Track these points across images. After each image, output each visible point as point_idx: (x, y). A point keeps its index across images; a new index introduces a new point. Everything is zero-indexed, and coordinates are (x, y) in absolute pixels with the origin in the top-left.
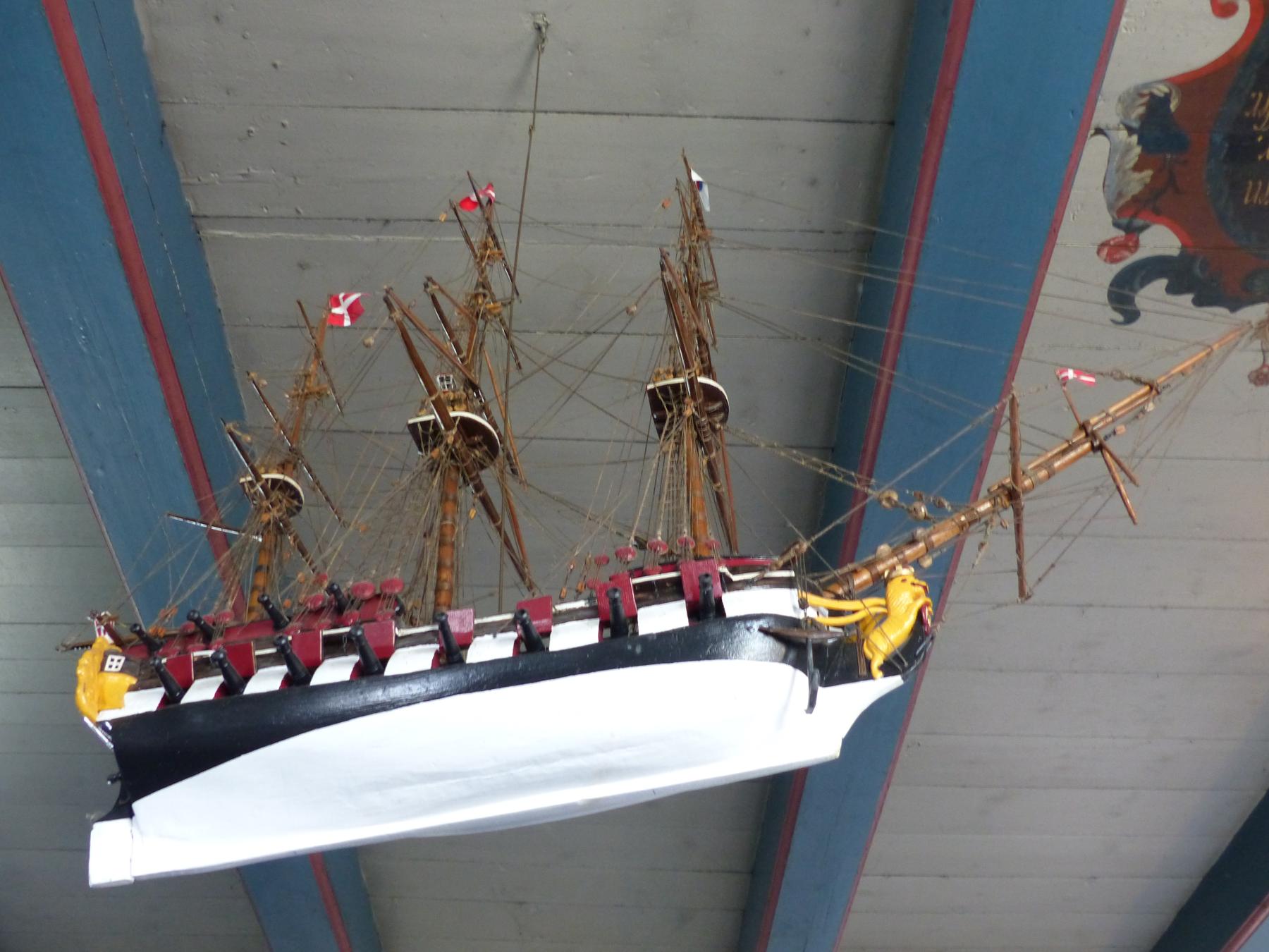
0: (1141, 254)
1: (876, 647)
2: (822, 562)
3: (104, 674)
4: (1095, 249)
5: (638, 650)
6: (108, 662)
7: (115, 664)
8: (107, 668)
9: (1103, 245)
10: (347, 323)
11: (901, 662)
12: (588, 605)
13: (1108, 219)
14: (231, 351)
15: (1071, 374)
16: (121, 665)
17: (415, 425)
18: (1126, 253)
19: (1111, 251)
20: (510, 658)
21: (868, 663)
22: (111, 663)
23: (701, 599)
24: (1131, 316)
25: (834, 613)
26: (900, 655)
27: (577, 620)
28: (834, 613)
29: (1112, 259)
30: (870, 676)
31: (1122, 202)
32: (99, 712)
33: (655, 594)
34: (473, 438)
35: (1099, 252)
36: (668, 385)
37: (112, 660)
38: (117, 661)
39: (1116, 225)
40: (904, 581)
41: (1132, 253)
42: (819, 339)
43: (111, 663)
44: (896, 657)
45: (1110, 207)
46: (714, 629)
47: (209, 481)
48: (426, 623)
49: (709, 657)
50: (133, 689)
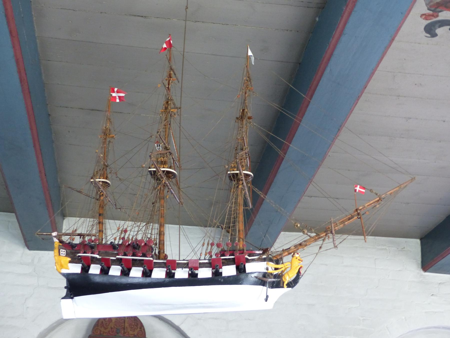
0: (440, 18)
1: (286, 279)
2: (285, 114)
3: (60, 256)
4: (420, 15)
5: (222, 280)
6: (61, 252)
7: (63, 253)
8: (61, 254)
9: (423, 15)
10: (118, 101)
11: (292, 284)
12: (208, 262)
13: (426, 8)
14: (33, 13)
15: (358, 188)
16: (65, 253)
17: (151, 171)
18: (433, 18)
19: (425, 16)
20: (187, 278)
21: (283, 283)
22: (63, 251)
23: (241, 279)
24: (434, 35)
25: (276, 269)
26: (292, 282)
27: (206, 267)
28: (276, 269)
29: (426, 19)
30: (283, 287)
31: (432, 4)
32: (61, 269)
33: (228, 262)
34: (169, 174)
35: (421, 17)
36: (234, 173)
37: (62, 251)
38: (63, 252)
39: (429, 9)
40: (297, 258)
41: (435, 18)
42: (298, 31)
43: (63, 251)
44: (291, 282)
45: (427, 5)
46: (243, 276)
47: (26, 74)
48: (162, 259)
49: (241, 284)
50: (70, 262)
